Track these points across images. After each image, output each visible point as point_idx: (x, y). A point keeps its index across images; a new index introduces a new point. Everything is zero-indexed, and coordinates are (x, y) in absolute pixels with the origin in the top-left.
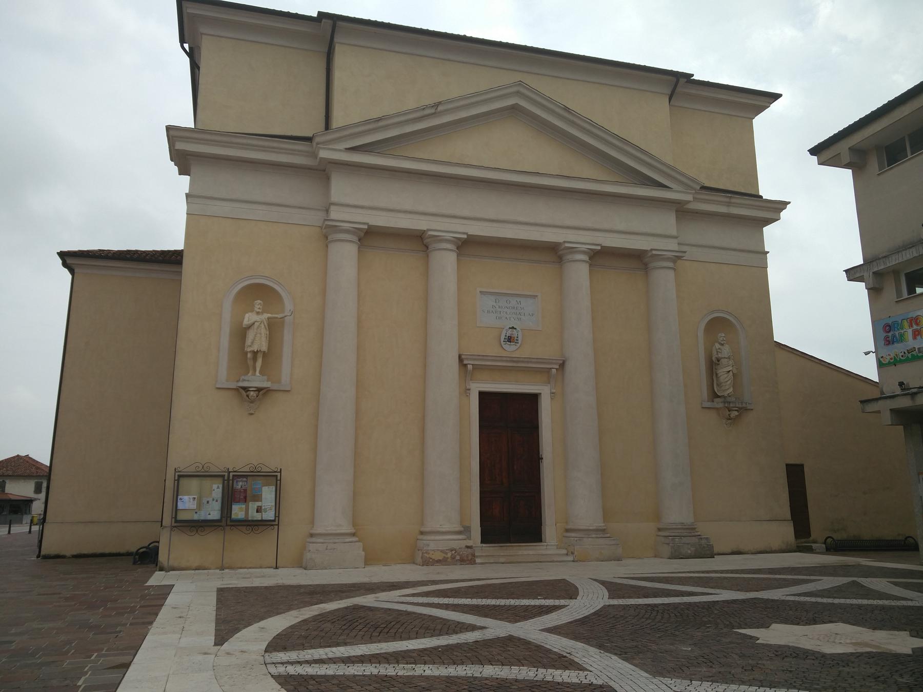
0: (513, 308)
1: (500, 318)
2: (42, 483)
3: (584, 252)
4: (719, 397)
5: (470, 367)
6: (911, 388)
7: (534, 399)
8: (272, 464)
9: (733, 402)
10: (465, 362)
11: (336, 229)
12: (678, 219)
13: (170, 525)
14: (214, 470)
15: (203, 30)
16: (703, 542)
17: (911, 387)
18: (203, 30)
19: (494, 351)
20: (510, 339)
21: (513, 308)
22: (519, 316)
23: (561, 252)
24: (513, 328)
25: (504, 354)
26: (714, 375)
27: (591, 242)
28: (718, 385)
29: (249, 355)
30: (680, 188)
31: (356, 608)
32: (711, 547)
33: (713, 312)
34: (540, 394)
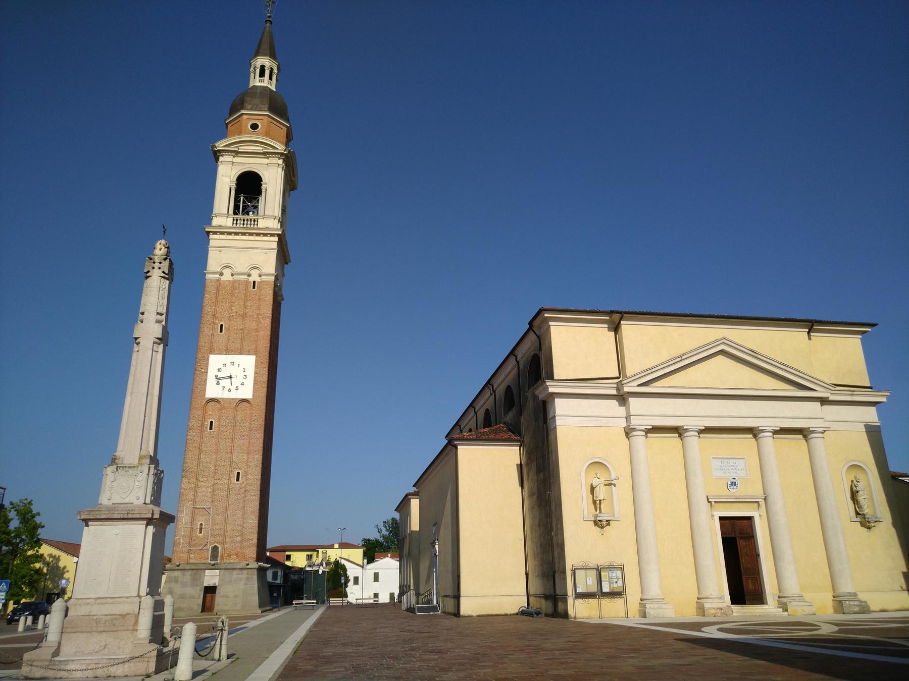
0: (732, 466)
1: (725, 473)
2: (277, 572)
3: (771, 432)
4: (860, 514)
5: (713, 503)
6: (521, 463)
7: (750, 519)
8: (617, 562)
9: (870, 518)
10: (710, 500)
11: (634, 430)
12: (822, 405)
13: (137, 593)
14: (591, 565)
15: (551, 323)
16: (863, 604)
17: (519, 463)
18: (551, 323)
19: (724, 492)
20: (734, 484)
21: (732, 466)
22: (736, 471)
23: (756, 432)
24: (734, 478)
25: (730, 494)
26: (855, 501)
27: (773, 425)
28: (858, 507)
29: (598, 502)
30: (823, 390)
31: (848, 645)
32: (868, 606)
33: (853, 461)
34: (753, 517)
